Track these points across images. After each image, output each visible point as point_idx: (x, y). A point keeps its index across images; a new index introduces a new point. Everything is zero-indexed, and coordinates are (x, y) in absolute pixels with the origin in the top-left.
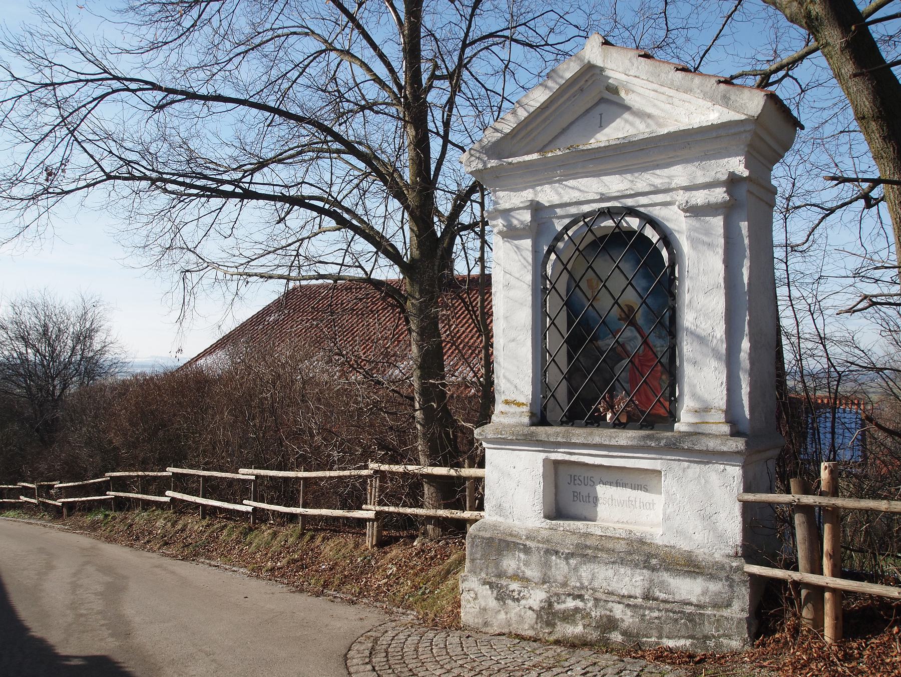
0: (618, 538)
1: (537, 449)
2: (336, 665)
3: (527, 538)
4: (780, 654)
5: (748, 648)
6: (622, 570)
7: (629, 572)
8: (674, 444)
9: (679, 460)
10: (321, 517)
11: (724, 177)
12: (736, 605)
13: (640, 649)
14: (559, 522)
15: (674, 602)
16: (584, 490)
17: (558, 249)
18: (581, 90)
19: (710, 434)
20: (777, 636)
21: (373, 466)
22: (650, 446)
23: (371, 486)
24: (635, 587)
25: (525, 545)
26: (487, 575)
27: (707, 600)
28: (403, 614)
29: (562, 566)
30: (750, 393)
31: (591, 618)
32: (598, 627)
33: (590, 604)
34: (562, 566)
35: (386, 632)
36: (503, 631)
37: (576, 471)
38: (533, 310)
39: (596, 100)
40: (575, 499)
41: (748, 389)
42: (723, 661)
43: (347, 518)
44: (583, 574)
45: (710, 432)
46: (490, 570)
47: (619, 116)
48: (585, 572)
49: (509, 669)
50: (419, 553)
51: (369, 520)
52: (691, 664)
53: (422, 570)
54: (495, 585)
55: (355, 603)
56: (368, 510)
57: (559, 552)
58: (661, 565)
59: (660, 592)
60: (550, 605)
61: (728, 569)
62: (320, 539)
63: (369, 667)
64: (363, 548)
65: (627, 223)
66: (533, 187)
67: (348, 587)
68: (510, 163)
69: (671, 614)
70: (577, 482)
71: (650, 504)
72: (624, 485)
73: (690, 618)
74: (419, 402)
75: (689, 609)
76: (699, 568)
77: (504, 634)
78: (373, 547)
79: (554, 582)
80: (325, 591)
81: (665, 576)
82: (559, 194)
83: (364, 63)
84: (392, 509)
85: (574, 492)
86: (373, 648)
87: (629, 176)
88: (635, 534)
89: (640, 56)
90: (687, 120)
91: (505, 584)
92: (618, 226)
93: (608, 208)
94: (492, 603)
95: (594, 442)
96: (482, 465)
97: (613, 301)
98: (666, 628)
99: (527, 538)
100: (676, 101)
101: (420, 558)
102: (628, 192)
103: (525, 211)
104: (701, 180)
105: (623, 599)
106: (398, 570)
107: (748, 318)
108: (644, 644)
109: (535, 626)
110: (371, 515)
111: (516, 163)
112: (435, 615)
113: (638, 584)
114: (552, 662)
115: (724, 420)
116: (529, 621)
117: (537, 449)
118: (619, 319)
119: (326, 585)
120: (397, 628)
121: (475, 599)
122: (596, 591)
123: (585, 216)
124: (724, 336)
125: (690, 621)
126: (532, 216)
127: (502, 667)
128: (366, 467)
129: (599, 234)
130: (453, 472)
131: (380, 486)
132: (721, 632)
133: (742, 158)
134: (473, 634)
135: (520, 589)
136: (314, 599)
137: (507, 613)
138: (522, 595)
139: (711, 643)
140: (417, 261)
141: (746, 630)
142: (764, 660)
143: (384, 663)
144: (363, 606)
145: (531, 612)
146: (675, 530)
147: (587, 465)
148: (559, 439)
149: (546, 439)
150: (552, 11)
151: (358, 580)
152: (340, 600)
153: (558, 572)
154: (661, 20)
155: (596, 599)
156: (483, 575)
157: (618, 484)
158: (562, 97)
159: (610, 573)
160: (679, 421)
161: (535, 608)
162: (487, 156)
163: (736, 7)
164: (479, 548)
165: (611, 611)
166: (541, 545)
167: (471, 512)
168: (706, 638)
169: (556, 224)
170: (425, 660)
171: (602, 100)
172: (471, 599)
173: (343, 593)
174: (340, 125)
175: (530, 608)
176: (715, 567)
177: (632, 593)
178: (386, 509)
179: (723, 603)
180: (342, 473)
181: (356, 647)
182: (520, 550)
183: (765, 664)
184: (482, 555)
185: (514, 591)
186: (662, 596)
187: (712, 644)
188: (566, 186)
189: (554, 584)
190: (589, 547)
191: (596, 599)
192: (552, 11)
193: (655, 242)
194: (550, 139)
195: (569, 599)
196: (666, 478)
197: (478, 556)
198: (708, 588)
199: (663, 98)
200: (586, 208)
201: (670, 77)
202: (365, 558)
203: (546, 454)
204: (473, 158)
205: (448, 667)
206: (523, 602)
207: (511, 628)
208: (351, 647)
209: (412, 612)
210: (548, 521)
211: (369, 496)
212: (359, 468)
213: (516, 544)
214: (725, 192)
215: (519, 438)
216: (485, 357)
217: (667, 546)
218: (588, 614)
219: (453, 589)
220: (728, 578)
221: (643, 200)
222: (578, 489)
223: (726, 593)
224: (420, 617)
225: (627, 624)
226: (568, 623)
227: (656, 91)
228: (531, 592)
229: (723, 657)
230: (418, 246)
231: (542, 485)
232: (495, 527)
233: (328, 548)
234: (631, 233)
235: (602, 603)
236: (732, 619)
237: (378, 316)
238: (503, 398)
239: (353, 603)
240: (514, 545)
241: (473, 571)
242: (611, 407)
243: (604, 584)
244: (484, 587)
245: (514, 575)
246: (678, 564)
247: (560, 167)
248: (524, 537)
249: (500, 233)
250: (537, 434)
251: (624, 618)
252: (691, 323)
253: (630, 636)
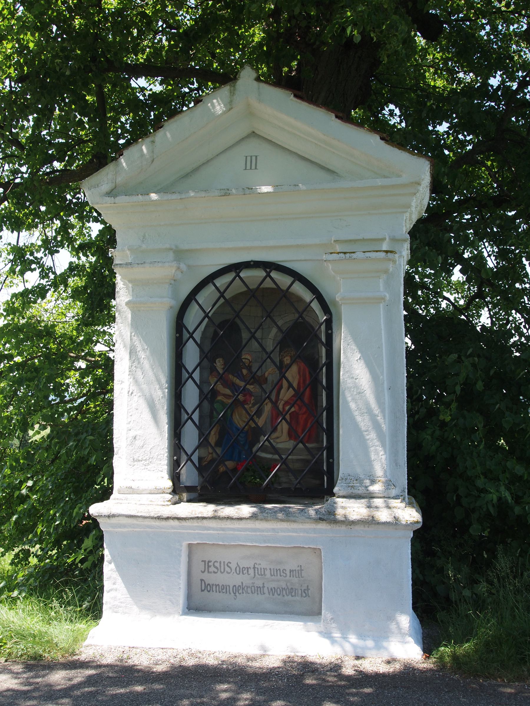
70: (212, 569)
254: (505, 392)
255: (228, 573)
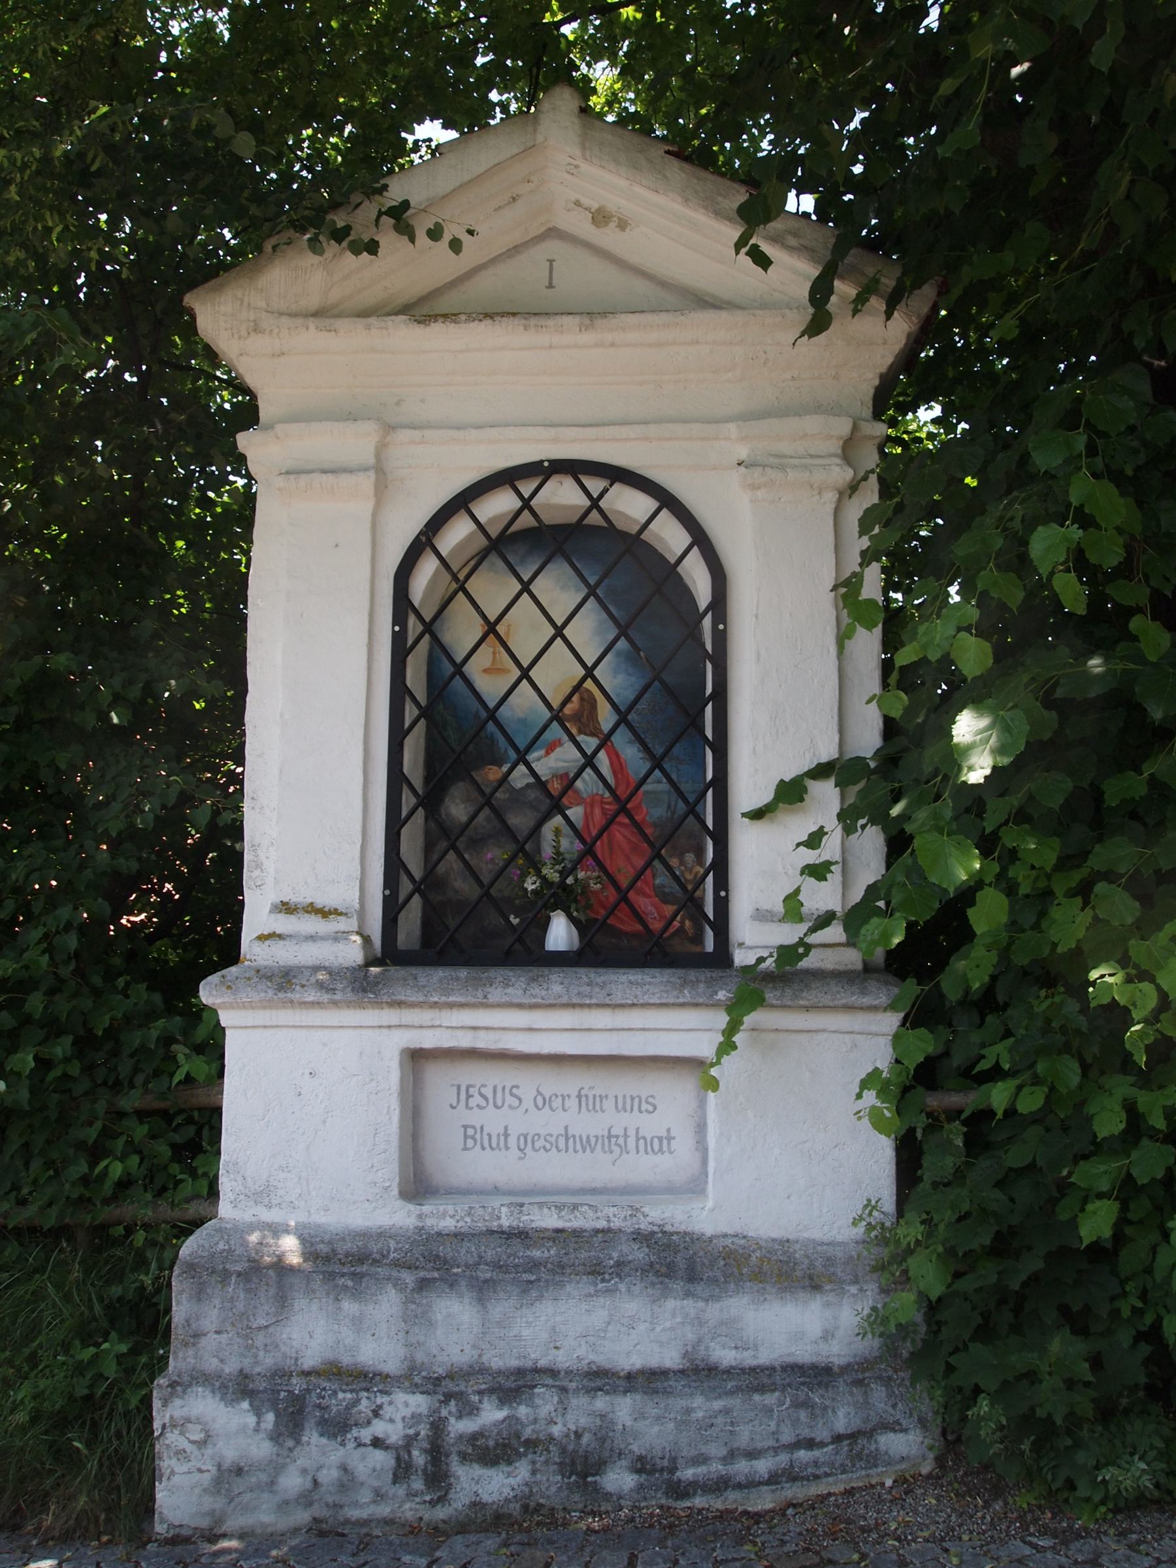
59: (724, 1347)
70: (476, 1100)
71: (660, 1139)
85: (465, 1127)
172: (189, 1448)
176: (424, 1374)
251: (640, 1425)
254: (835, 16)
255: (510, 1107)
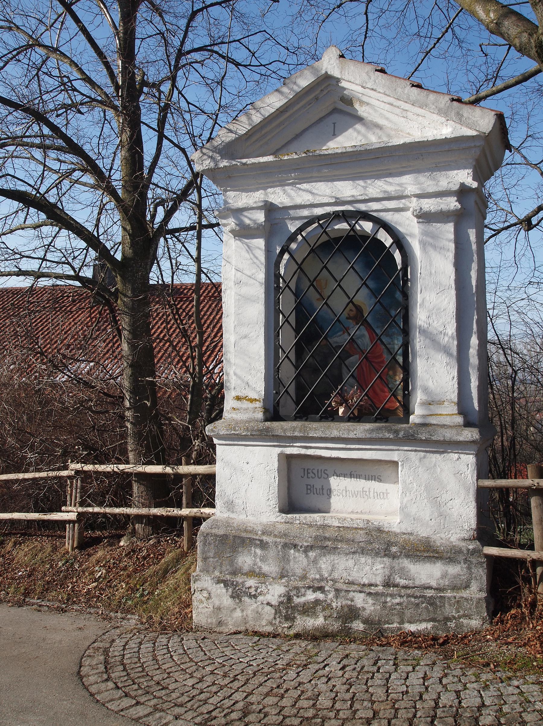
0: (356, 528)
1: (272, 444)
2: (73, 686)
3: (263, 533)
4: (521, 630)
5: (487, 626)
6: (363, 560)
7: (370, 561)
8: (412, 435)
9: (416, 451)
10: (12, 522)
11: (456, 187)
12: (474, 586)
13: (383, 636)
14: (295, 515)
15: (414, 588)
16: (317, 483)
17: (291, 249)
18: (317, 98)
19: (444, 425)
20: (513, 612)
21: (75, 466)
22: (388, 438)
23: (71, 487)
24: (376, 575)
25: (261, 541)
26: (221, 573)
27: (447, 583)
28: (123, 619)
29: (301, 559)
30: (479, 387)
31: (332, 609)
32: (339, 617)
33: (331, 595)
34: (301, 559)
35: (113, 641)
36: (239, 629)
37: (309, 465)
38: (265, 307)
39: (330, 109)
40: (309, 491)
41: (477, 383)
42: (466, 641)
43: (44, 521)
44: (323, 566)
45: (445, 423)
46: (224, 568)
47: (351, 126)
48: (325, 564)
49: (263, 671)
50: (129, 553)
51: (69, 522)
52: (437, 647)
53: (135, 571)
54: (229, 583)
55: (66, 611)
56: (68, 512)
57: (298, 545)
58: (401, 552)
59: (401, 578)
60: (289, 599)
61: (465, 552)
62: (11, 544)
63: (111, 685)
64: (62, 551)
65: (361, 226)
66: (265, 189)
67: (54, 593)
68: (245, 164)
69: (413, 600)
70: (311, 475)
71: (383, 493)
72: (358, 477)
73: (431, 601)
74: (129, 401)
75: (429, 593)
76: (437, 553)
77: (240, 632)
78: (73, 549)
79: (292, 576)
80: (27, 600)
81: (406, 563)
82: (289, 196)
83: (73, 62)
84: (97, 509)
85: (307, 485)
86: (106, 662)
87: (361, 183)
88: (372, 524)
89: (376, 70)
90: (419, 134)
91: (240, 580)
92: (353, 229)
93: (343, 211)
94: (227, 602)
95: (332, 436)
96: (212, 461)
97: (348, 301)
98: (408, 613)
99: (263, 533)
100: (410, 115)
101: (131, 558)
102: (360, 198)
103: (259, 211)
104: (431, 190)
105: (364, 588)
106: (108, 572)
107: (476, 317)
108: (385, 630)
109: (274, 622)
110: (72, 516)
111: (250, 164)
112: (161, 618)
113: (378, 572)
114: (304, 659)
115: (457, 412)
116: (267, 617)
117: (272, 444)
118: (347, 318)
119: (27, 594)
120: (124, 636)
121: (209, 598)
122: (336, 582)
123: (319, 218)
124: (455, 333)
125: (431, 604)
126: (266, 217)
127: (256, 669)
128: (66, 468)
129: (333, 236)
130: (169, 470)
131: (82, 488)
132: (462, 613)
133: (470, 171)
134: (207, 634)
135: (257, 585)
136: (15, 611)
137: (242, 611)
138: (259, 591)
139: (452, 624)
140: (130, 259)
141: (485, 609)
142: (508, 636)
143: (126, 678)
144: (75, 613)
145: (269, 608)
146: (412, 518)
147: (320, 458)
148: (297, 434)
149: (282, 434)
150: (265, 31)
151: (63, 585)
152: (46, 609)
153: (296, 566)
154: (358, 53)
155: (337, 591)
156: (217, 573)
157: (351, 476)
158: (298, 103)
159: (351, 563)
160: (413, 413)
161: (273, 603)
162: (221, 156)
163: (435, 44)
164: (212, 546)
165: (352, 600)
166: (278, 540)
167: (190, 510)
168: (447, 619)
169: (289, 226)
170: (170, 670)
171: (335, 110)
172: (203, 599)
173: (49, 600)
174: (58, 116)
175: (268, 604)
176: (453, 551)
177: (373, 581)
178: (90, 510)
179: (461, 584)
180: (37, 475)
181: (86, 662)
182: (256, 546)
183: (509, 640)
184: (215, 553)
185: (250, 587)
186: (403, 582)
187: (453, 625)
188: (300, 189)
189: (292, 578)
190: (329, 539)
191: (337, 591)
192: (265, 31)
193: (388, 246)
194: (283, 143)
195: (309, 592)
196: (403, 468)
197: (211, 554)
198: (447, 571)
199: (398, 111)
200: (319, 211)
201: (406, 92)
202: (67, 562)
203: (281, 449)
204: (205, 157)
205: (198, 675)
206: (260, 598)
207: (248, 625)
208: (81, 662)
209: (133, 616)
210: (284, 515)
211: (68, 497)
212: (59, 469)
213: (251, 540)
214: (456, 201)
215: (254, 433)
216: (198, 356)
217: (404, 534)
218: (329, 605)
219: (176, 589)
220: (466, 560)
221: (374, 206)
222: (311, 482)
223: (464, 575)
224: (144, 621)
225: (368, 612)
226: (308, 615)
227: (392, 105)
228: (269, 587)
229: (465, 637)
230: (131, 245)
231: (277, 479)
232: (228, 524)
233: (21, 554)
234: (364, 237)
235: (343, 594)
236: (471, 600)
237: (52, 320)
238: (233, 394)
239: (64, 611)
240: (250, 541)
241: (206, 570)
242: (344, 401)
243: (345, 575)
244: (218, 586)
245: (250, 571)
246: (418, 551)
247: (295, 170)
248: (260, 532)
249: (232, 231)
250: (273, 430)
251: (366, 606)
252: (424, 322)
253: (371, 624)
